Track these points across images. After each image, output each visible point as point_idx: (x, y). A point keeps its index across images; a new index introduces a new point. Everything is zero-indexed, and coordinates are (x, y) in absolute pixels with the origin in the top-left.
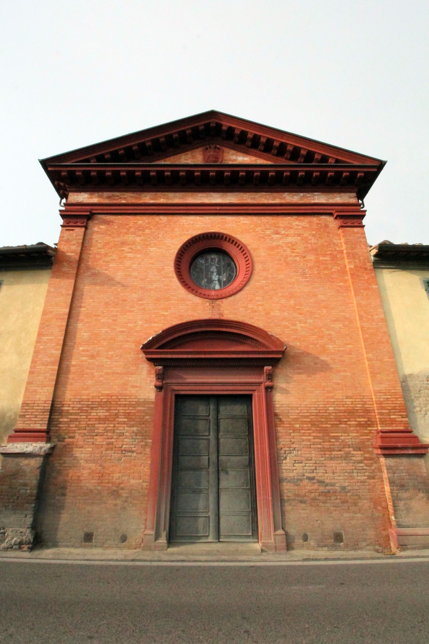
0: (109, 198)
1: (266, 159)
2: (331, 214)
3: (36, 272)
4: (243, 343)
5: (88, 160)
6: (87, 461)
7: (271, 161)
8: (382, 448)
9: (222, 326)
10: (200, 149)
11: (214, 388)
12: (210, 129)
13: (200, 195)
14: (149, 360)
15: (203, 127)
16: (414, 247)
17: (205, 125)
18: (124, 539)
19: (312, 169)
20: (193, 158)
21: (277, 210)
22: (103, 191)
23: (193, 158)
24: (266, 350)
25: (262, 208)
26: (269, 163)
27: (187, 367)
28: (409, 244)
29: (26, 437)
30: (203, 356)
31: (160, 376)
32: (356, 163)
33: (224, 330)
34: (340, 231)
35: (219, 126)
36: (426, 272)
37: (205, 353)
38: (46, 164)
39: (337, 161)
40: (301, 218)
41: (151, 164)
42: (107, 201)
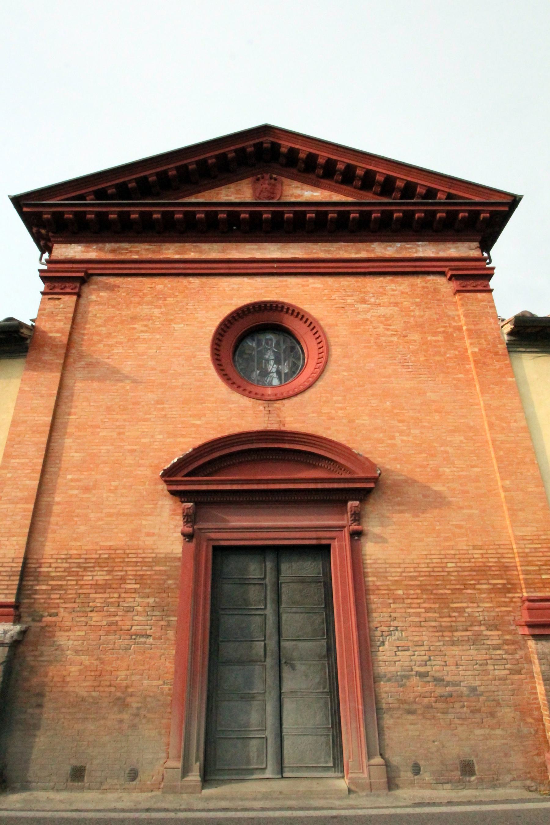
0: (113, 251)
2: (442, 273)
4: (315, 467)
7: (352, 196)
9: (283, 441)
12: (262, 151)
13: (249, 246)
14: (173, 493)
18: (133, 775)
19: (41, 209)
20: (238, 193)
23: (238, 193)
26: (350, 199)
30: (255, 487)
31: (190, 518)
33: (287, 446)
35: (275, 147)
42: (110, 257)
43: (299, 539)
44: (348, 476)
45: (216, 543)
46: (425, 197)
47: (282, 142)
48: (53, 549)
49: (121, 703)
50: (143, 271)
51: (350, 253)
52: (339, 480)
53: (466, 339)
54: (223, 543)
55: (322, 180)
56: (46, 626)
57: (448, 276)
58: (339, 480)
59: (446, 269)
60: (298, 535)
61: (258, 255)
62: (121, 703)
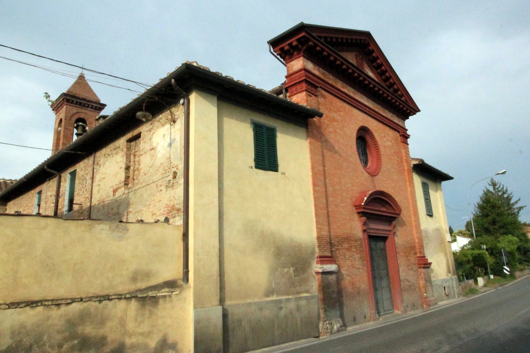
0: (323, 74)
1: (377, 77)
2: (399, 132)
3: (299, 128)
4: (384, 206)
5: (320, 37)
8: (418, 264)
9: (384, 196)
10: (354, 54)
12: (362, 43)
14: (359, 213)
16: (428, 165)
17: (373, 49)
19: (319, 44)
20: (351, 58)
21: (327, 87)
23: (351, 58)
27: (377, 219)
29: (324, 261)
31: (365, 224)
32: (411, 106)
33: (383, 198)
35: (368, 45)
36: (290, 135)
37: (374, 210)
42: (322, 77)
44: (393, 212)
45: (370, 234)
46: (399, 95)
50: (326, 89)
54: (372, 234)
56: (139, 326)
58: (390, 213)
59: (401, 131)
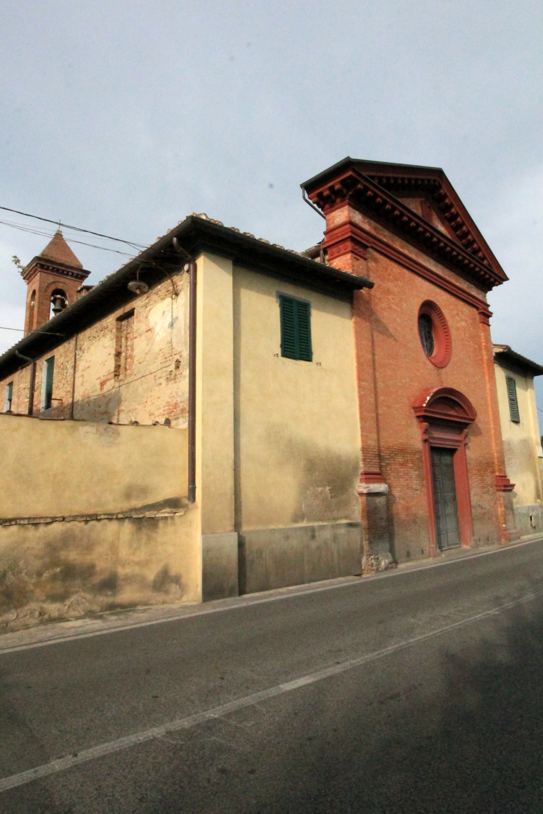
0: (375, 229)
2: (477, 308)
4: (453, 408)
6: (399, 498)
7: (451, 237)
8: (496, 486)
9: (455, 396)
10: (419, 200)
11: (447, 443)
13: (411, 248)
14: (418, 417)
15: (443, 194)
18: (423, 552)
20: (415, 206)
22: (371, 218)
24: (467, 417)
25: (419, 267)
26: (449, 237)
28: (225, 226)
30: (448, 418)
31: (426, 432)
33: (453, 398)
34: (480, 324)
35: (440, 187)
38: (507, 279)
39: (489, 265)
40: (467, 306)
41: (394, 197)
42: (373, 232)
43: (441, 444)
45: (433, 445)
46: (480, 258)
47: (443, 186)
48: (75, 400)
49: (415, 522)
51: (457, 282)
52: (462, 418)
53: (483, 350)
55: (446, 221)
57: (480, 311)
59: (480, 307)
60: (451, 443)
61: (453, 281)
62: (415, 522)
